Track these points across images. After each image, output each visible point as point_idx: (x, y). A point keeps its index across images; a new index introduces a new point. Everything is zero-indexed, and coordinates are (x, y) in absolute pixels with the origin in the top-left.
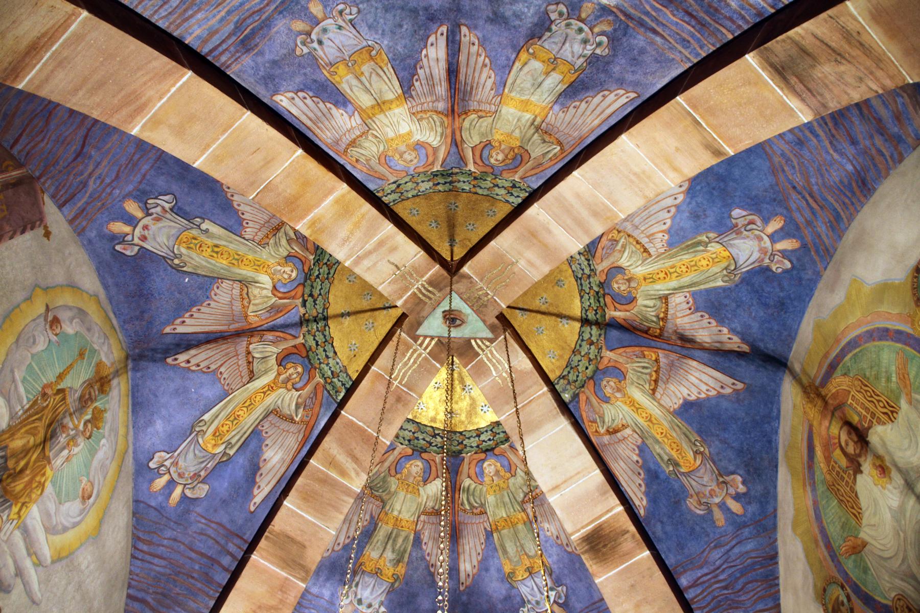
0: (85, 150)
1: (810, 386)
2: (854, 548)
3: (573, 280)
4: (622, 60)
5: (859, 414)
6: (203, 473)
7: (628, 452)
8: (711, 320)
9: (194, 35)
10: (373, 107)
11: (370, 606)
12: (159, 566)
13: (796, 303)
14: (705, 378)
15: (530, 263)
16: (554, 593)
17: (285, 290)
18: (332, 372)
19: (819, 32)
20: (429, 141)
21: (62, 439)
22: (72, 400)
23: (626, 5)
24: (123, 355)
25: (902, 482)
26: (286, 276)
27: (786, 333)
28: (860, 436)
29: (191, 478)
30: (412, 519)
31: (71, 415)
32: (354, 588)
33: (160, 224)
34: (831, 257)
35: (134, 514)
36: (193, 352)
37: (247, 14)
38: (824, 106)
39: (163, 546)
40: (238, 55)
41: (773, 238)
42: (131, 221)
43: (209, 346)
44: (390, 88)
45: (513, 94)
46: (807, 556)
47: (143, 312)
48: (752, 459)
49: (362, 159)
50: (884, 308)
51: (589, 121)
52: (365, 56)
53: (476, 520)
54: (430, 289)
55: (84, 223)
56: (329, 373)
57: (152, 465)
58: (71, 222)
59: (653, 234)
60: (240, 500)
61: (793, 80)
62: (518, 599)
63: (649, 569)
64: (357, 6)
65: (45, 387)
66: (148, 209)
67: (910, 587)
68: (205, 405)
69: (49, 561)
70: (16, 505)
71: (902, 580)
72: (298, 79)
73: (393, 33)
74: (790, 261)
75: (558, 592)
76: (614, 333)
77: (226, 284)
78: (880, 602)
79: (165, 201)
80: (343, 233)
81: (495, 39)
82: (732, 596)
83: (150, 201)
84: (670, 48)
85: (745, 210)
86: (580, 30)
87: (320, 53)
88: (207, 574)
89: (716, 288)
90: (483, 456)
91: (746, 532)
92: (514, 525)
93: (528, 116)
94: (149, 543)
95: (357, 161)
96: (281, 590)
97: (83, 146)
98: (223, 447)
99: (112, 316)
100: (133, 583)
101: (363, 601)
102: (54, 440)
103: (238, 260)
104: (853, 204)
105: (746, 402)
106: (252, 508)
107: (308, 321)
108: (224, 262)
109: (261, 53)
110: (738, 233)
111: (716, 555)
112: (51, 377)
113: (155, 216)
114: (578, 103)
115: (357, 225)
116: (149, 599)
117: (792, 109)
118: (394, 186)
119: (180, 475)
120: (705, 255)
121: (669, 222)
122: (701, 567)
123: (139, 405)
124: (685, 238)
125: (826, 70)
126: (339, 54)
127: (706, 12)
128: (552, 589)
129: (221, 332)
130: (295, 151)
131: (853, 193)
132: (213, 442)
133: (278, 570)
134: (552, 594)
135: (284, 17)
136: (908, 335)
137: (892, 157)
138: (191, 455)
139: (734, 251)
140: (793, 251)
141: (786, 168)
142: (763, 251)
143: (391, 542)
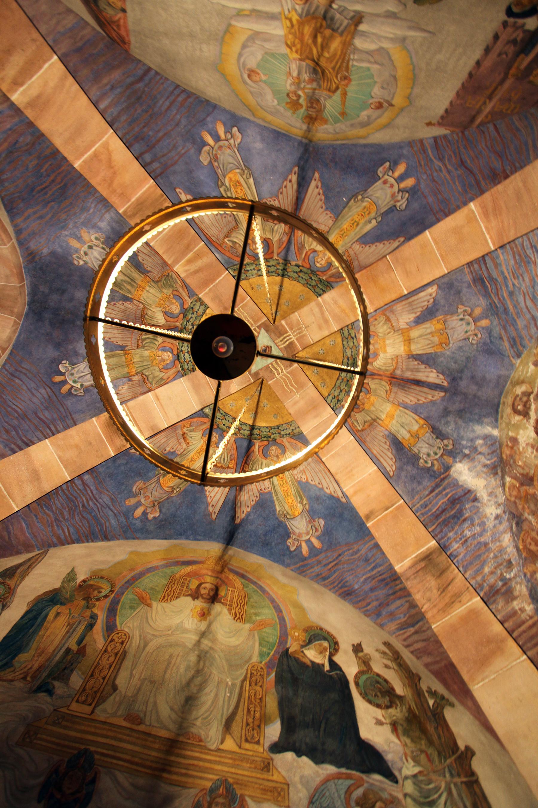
0: (463, 168)
1: (225, 561)
2: (143, 598)
3: (278, 424)
4: (414, 471)
5: (226, 596)
6: (216, 164)
7: (171, 445)
8: (254, 502)
9: (501, 255)
10: (409, 336)
11: (86, 254)
12: (163, 103)
13: (268, 552)
14: (218, 495)
15: (296, 403)
16: (79, 386)
17: (310, 257)
18: (248, 271)
19: (456, 581)
20: (378, 362)
21: (306, 76)
22: (322, 94)
23: (450, 480)
24: (315, 139)
25: (203, 629)
26: (319, 260)
27: (249, 545)
28: (214, 598)
29: (216, 154)
30: (142, 298)
31: (315, 89)
32: (101, 246)
33: (389, 196)
34: (300, 574)
35: (207, 101)
36: (295, 186)
37: (499, 287)
38: (407, 579)
39: (176, 114)
40: (474, 274)
41: (308, 541)
42: (401, 179)
43: (295, 198)
44: (417, 348)
45: (398, 411)
46: (119, 563)
47: (336, 163)
48: (170, 523)
49: (376, 322)
50: (291, 609)
51: (376, 448)
52: (444, 340)
53: (134, 342)
54: (288, 343)
55: (415, 149)
56: (248, 269)
57: (235, 129)
58: (421, 141)
59: (305, 472)
60: (187, 184)
61: (423, 564)
62: (75, 361)
63: (102, 455)
64: (477, 344)
65: (350, 80)
66: (402, 192)
67: (138, 642)
68: (259, 182)
69: (234, 23)
70: (297, 20)
71: (140, 636)
72: (442, 302)
73: (453, 358)
74: (295, 550)
75: (79, 389)
76: (245, 444)
77: (330, 222)
78: (116, 620)
79: (402, 204)
80: (341, 302)
81: (434, 409)
82: (78, 510)
83: (407, 195)
84: (421, 498)
85: (324, 526)
86: (436, 454)
87: (455, 318)
88: (143, 139)
89: (274, 506)
90: (175, 353)
91: (123, 519)
92: (128, 366)
93: (383, 417)
94: (182, 104)
95: (376, 319)
96: (122, 194)
97: (466, 168)
98: (228, 185)
99: (343, 142)
100: (158, 77)
101: (91, 250)
102: (311, 70)
103: (342, 235)
104: (334, 587)
105: (204, 520)
106: (178, 190)
107: (286, 265)
108: (345, 226)
109: (469, 286)
110: (310, 522)
111: (106, 499)
112: (352, 89)
113: (396, 194)
114: (388, 444)
115: (343, 311)
116: (140, 85)
117: (403, 561)
118: (353, 335)
119: (221, 147)
120: (295, 502)
121: (313, 483)
122: (97, 489)
123: (278, 136)
124: (304, 492)
125: (432, 582)
126: (450, 327)
127: (444, 521)
128: (82, 385)
129: (300, 209)
130: (407, 290)
131: (341, 588)
132: (233, 179)
133: (137, 196)
134: (78, 385)
135: (487, 305)
136: (286, 626)
137: (367, 610)
138: (231, 160)
139: (298, 518)
140: (301, 552)
141: (351, 551)
142: (300, 535)
143: (129, 280)
